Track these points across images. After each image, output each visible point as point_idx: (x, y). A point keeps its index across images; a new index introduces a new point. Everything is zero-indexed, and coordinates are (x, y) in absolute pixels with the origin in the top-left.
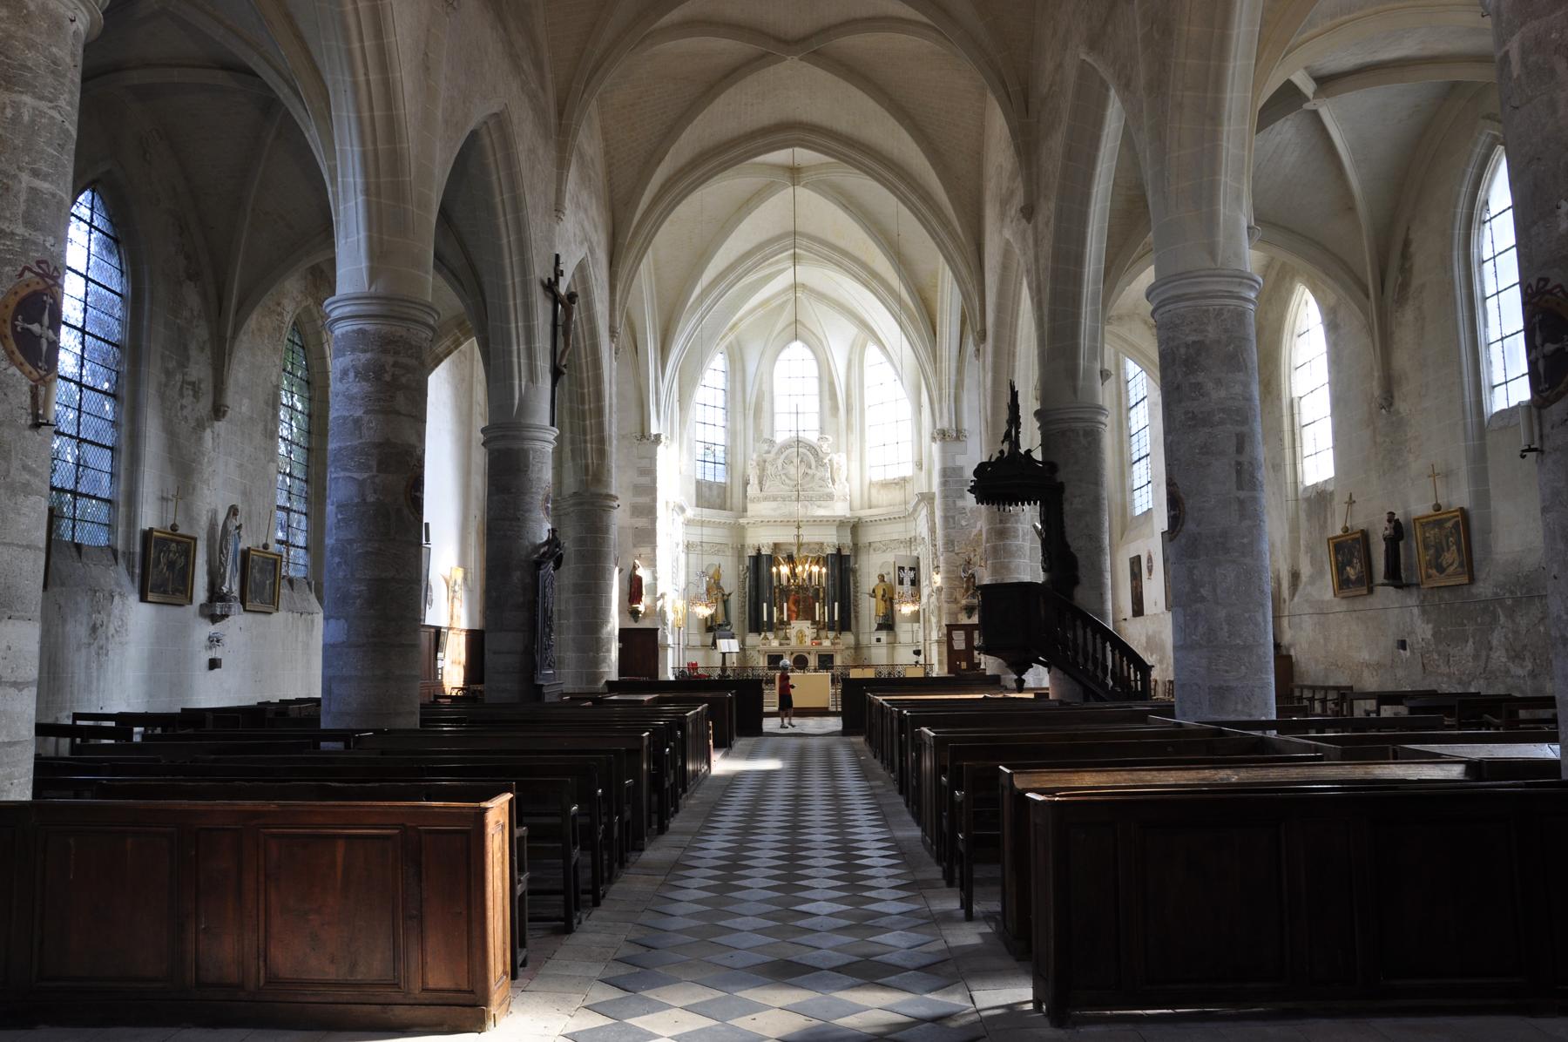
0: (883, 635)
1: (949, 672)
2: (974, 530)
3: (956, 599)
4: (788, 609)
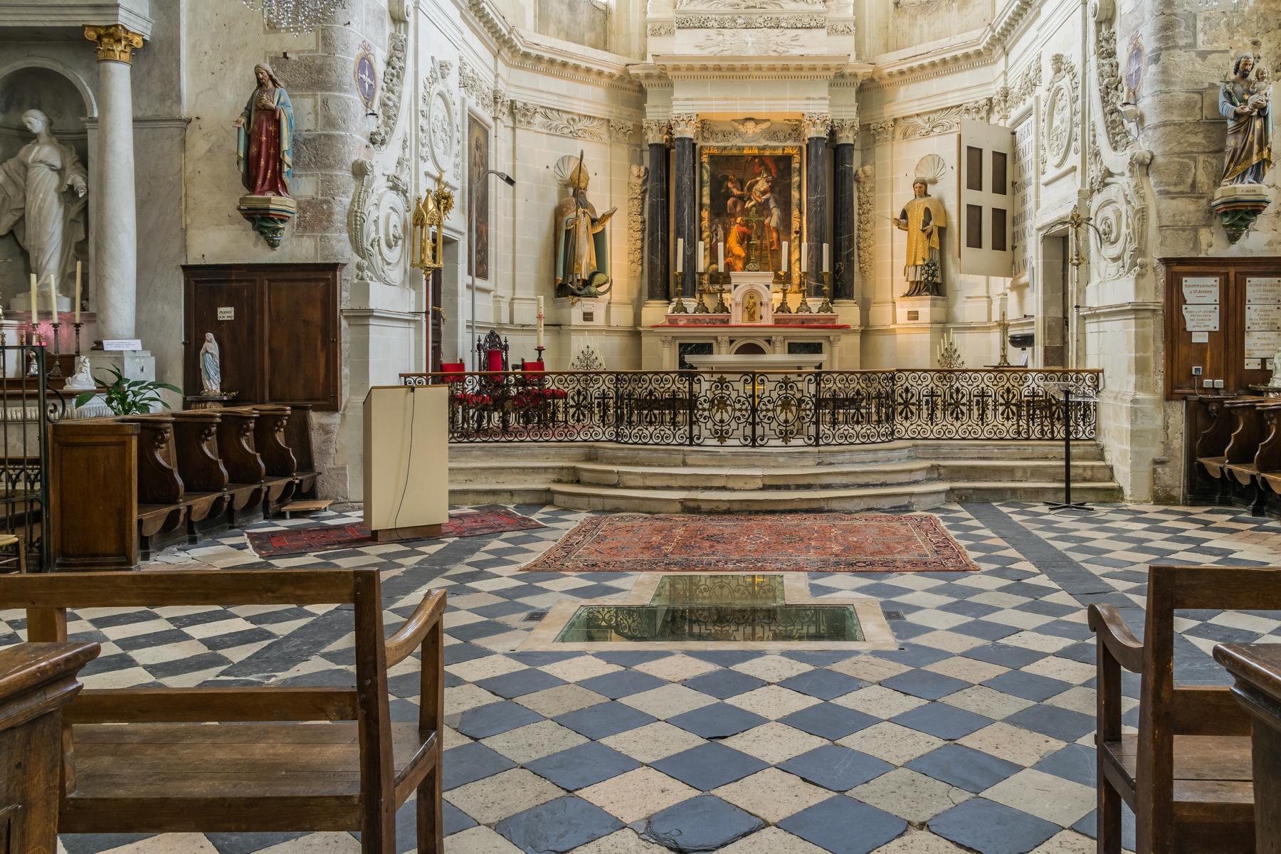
0: (924, 306)
3: (1193, 185)
4: (728, 252)
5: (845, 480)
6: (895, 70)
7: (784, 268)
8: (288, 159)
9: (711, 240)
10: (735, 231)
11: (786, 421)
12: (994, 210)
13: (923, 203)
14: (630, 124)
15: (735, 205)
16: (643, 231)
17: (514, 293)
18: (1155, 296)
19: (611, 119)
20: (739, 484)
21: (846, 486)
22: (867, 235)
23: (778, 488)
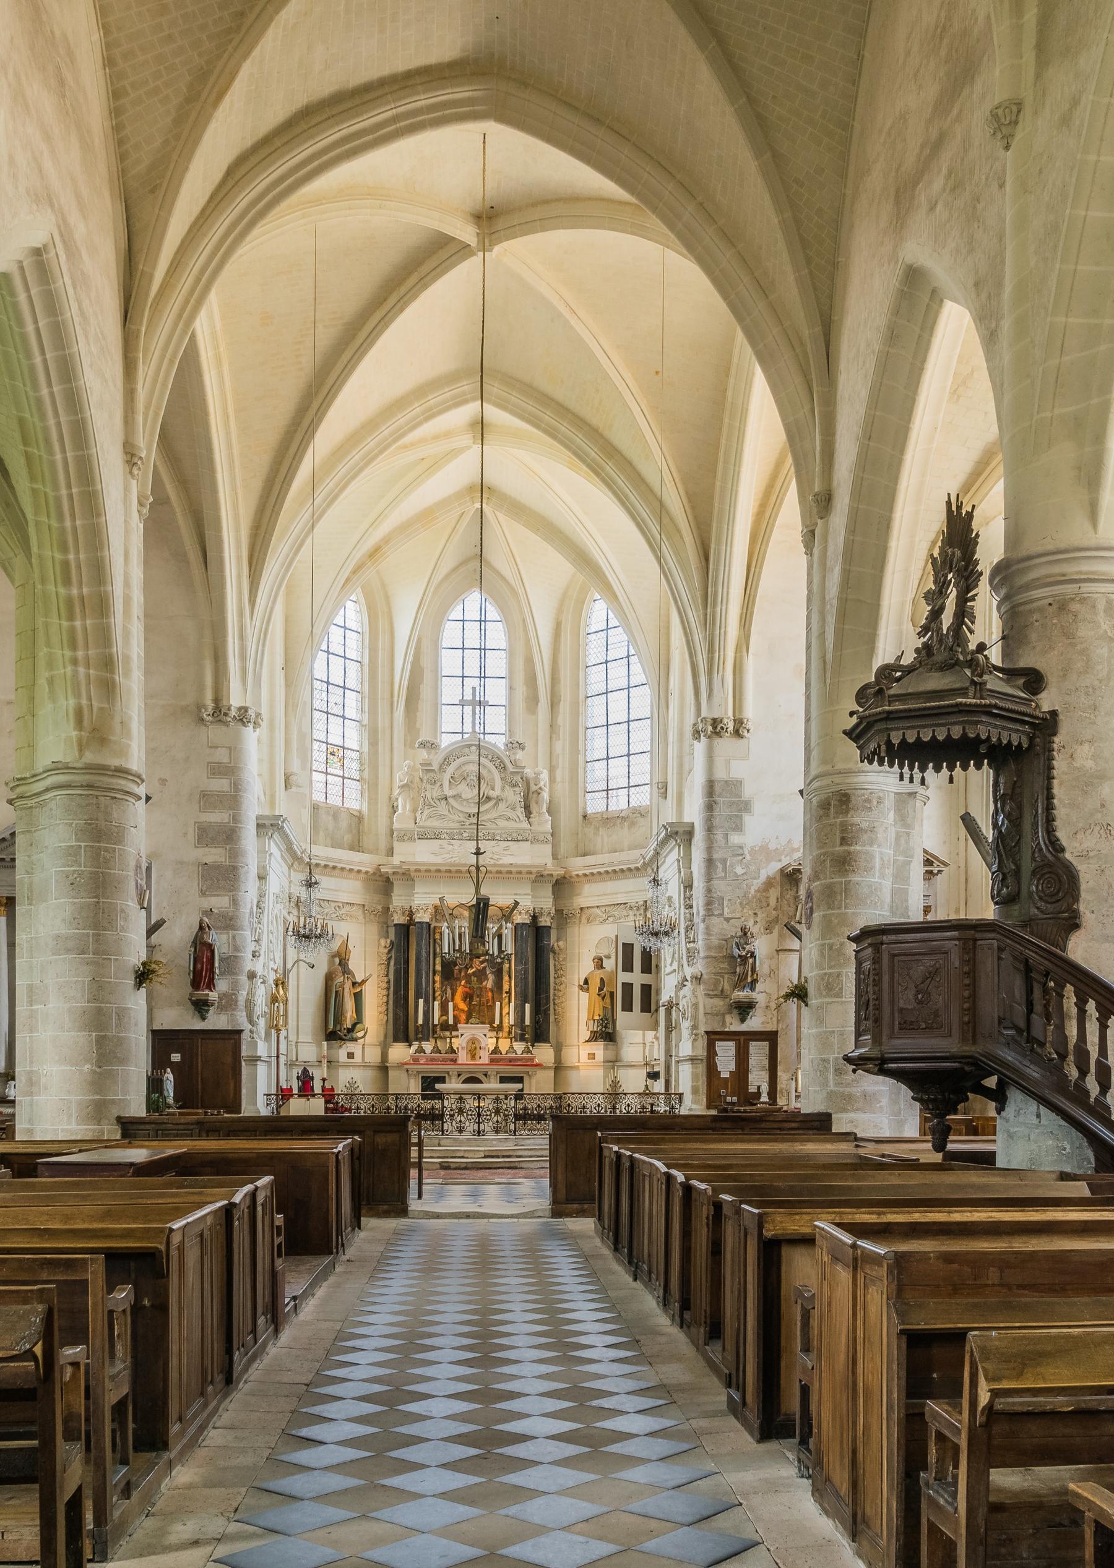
0: (599, 1049)
1: (709, 1107)
2: (755, 882)
3: (722, 991)
4: (455, 1007)
5: (530, 1153)
6: (580, 873)
7: (497, 1022)
8: (217, 971)
9: (442, 998)
10: (460, 991)
11: (497, 1121)
12: (642, 985)
13: (600, 974)
14: (380, 908)
15: (460, 971)
16: (388, 989)
17: (298, 1038)
18: (702, 1052)
19: (366, 904)
20: (471, 1155)
21: (531, 1156)
22: (560, 994)
23: (493, 1157)
